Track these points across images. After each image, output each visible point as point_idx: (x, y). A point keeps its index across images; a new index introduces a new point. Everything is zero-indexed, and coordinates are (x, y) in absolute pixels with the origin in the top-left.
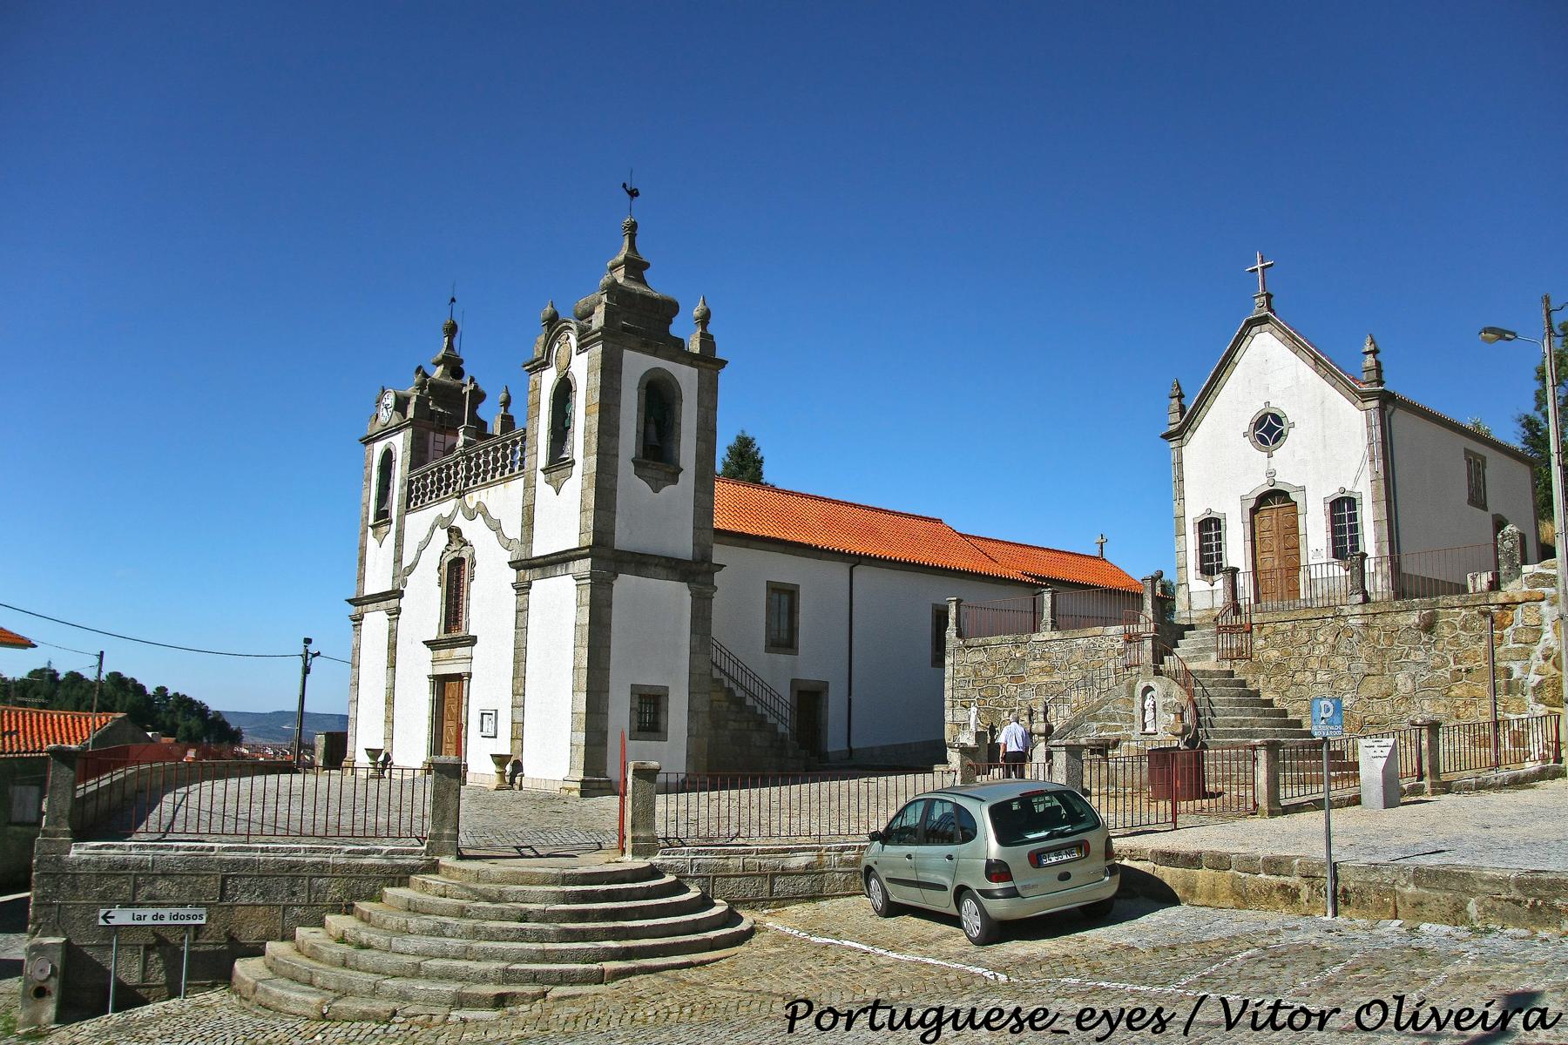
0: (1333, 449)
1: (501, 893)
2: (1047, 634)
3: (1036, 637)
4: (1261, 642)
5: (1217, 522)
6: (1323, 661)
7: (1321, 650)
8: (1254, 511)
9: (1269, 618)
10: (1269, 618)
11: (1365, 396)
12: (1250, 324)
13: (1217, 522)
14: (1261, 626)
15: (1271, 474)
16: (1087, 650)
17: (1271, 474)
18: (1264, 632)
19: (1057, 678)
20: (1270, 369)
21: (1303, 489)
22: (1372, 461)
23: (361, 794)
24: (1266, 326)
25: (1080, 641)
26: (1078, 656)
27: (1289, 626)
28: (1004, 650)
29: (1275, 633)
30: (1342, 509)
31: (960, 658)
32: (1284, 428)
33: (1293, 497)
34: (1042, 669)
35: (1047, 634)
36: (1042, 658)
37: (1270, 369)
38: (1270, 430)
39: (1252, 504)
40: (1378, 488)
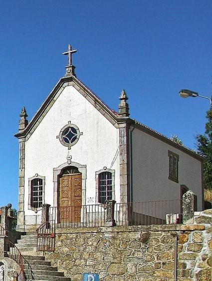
0: (101, 146)
7: (90, 249)
8: (60, 176)
11: (119, 121)
17: (69, 158)
18: (61, 238)
20: (72, 105)
22: (121, 154)
24: (71, 83)
32: (78, 135)
37: (72, 105)
39: (59, 172)
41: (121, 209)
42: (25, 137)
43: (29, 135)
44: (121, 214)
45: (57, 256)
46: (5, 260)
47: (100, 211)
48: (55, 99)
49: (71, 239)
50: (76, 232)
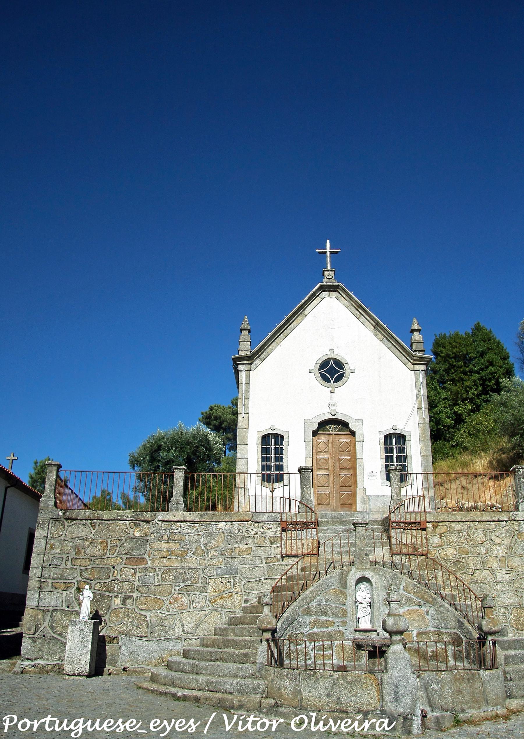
0: (389, 393)
1: (194, 666)
2: (177, 512)
3: (162, 516)
4: (435, 540)
5: (280, 438)
6: (503, 560)
7: (499, 551)
8: (315, 433)
9: (445, 517)
10: (445, 517)
11: (416, 360)
12: (323, 288)
13: (280, 438)
14: (436, 524)
15: (332, 406)
16: (231, 534)
17: (332, 406)
18: (438, 531)
19: (190, 563)
20: (329, 323)
21: (36, 463)
22: (420, 409)
23: (82, 488)
24: (335, 294)
25: (221, 525)
26: (220, 542)
27: (464, 526)
28: (120, 526)
29: (451, 531)
30: (394, 443)
31: (54, 530)
32: (318, 372)
33: (352, 427)
34: (170, 552)
35: (177, 512)
36: (170, 539)
37: (329, 323)
38: (332, 372)
39: (315, 427)
40: (424, 430)
41: (426, 493)
42: (251, 364)
43: (257, 361)
44: (427, 500)
45: (436, 564)
46: (374, 571)
47: (258, 494)
48: (306, 312)
49: (459, 532)
50: (469, 519)
